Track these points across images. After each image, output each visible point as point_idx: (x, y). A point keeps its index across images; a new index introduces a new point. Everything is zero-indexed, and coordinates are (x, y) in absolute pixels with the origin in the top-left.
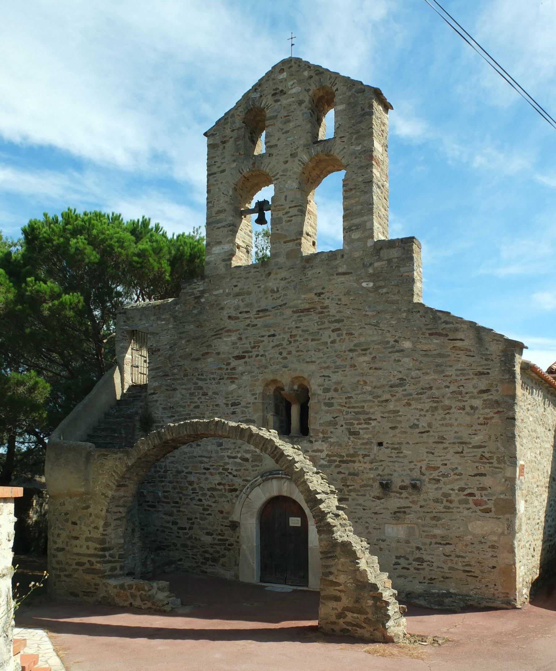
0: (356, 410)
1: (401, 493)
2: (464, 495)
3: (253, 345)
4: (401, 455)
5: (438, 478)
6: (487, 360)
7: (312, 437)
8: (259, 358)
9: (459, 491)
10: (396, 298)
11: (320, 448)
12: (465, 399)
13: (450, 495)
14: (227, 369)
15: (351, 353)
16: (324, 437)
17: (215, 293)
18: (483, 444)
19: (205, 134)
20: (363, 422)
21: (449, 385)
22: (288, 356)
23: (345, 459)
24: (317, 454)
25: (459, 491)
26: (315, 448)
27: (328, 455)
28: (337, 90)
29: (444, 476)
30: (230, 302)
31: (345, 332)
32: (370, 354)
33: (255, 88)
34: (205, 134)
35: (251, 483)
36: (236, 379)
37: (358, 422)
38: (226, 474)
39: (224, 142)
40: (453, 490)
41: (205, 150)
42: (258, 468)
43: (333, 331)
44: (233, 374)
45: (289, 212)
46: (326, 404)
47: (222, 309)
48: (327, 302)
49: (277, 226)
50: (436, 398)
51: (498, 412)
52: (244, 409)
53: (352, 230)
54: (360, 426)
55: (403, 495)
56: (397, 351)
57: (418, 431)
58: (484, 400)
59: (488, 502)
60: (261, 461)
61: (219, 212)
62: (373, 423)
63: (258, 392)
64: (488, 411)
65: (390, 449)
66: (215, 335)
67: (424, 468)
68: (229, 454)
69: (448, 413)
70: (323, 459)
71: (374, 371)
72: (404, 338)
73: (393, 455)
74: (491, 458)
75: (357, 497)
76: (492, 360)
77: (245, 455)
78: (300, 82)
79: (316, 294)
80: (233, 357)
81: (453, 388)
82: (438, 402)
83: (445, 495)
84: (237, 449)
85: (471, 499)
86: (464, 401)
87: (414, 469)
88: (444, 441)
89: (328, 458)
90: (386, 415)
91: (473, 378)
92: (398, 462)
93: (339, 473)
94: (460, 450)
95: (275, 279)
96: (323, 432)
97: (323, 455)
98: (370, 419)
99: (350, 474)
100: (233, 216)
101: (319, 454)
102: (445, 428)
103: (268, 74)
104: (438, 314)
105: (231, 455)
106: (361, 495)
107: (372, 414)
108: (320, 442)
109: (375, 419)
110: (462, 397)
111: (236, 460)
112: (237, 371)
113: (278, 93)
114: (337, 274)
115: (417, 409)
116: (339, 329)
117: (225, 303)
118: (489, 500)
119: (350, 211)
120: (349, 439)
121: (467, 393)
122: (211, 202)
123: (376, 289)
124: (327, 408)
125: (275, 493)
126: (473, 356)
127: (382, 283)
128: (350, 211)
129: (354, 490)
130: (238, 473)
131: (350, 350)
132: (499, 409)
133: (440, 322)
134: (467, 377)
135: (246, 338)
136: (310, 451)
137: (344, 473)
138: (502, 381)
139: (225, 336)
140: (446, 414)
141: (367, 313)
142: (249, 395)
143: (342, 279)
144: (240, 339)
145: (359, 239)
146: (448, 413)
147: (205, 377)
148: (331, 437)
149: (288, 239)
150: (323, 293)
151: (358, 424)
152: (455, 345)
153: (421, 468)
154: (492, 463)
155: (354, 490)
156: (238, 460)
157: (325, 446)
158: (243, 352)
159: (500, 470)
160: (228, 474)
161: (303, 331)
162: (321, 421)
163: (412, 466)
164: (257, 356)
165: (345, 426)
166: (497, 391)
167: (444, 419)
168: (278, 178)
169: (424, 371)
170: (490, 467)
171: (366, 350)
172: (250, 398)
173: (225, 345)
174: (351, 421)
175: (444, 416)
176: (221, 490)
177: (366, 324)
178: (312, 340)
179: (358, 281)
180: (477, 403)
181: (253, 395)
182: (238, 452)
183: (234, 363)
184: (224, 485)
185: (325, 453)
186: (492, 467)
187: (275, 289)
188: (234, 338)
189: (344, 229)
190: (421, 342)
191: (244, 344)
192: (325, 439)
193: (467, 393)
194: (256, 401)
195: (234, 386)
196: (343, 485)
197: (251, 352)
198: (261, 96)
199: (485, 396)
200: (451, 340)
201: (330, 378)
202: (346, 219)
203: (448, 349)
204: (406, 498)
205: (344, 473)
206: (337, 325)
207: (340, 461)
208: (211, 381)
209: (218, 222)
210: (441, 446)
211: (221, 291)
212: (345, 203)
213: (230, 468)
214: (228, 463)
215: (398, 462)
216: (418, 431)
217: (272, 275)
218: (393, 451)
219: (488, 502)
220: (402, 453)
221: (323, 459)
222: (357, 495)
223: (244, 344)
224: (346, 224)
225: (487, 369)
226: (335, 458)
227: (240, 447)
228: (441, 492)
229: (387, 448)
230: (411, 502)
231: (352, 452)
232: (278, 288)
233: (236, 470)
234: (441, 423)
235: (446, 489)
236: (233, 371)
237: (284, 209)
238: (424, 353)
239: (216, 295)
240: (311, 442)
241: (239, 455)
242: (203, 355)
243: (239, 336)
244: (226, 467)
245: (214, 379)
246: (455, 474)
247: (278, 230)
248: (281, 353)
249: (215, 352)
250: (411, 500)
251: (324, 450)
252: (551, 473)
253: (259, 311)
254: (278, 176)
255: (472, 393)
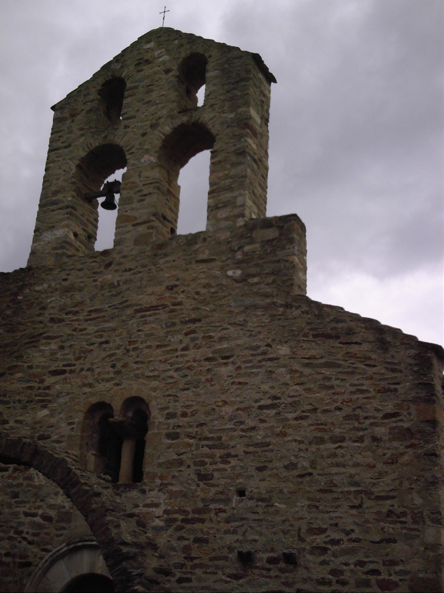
0: (210, 443)
1: (269, 570)
2: (364, 573)
3: (77, 355)
4: (271, 510)
5: (324, 545)
6: (393, 371)
7: (145, 484)
8: (84, 373)
9: (355, 565)
10: (268, 290)
11: (155, 501)
12: (363, 426)
13: (342, 572)
14: (39, 388)
15: (207, 363)
16: (162, 484)
17: (38, 288)
18: (391, 494)
19: (53, 108)
20: (219, 460)
21: (341, 406)
22: (123, 370)
23: (190, 516)
24: (151, 509)
25: (355, 565)
26: (148, 501)
27: (166, 512)
28: (210, 56)
29: (334, 542)
30: (54, 301)
31: (202, 335)
32: (233, 363)
33: (117, 59)
34: (53, 108)
35: (51, 553)
36: (50, 401)
37: (211, 460)
38: (19, 539)
39: (73, 116)
40: (346, 564)
41: (50, 123)
42: (64, 532)
43: (186, 334)
44: (47, 395)
45: (142, 190)
46: (169, 436)
47: (44, 308)
48: (181, 297)
49: (126, 206)
50: (322, 424)
51: (412, 446)
52: (55, 445)
53: (219, 208)
54: (215, 467)
55: (272, 573)
56: (271, 359)
57: (296, 472)
58: (392, 429)
59: (400, 583)
60: (69, 521)
61: (55, 193)
62: (233, 462)
63: (76, 420)
64: (395, 444)
65: (255, 500)
66: (29, 343)
67: (303, 530)
68: (26, 509)
69: (340, 447)
70: (158, 517)
71: (238, 386)
72: (280, 341)
73: (260, 510)
74: (404, 514)
75: (203, 575)
76: (401, 371)
77: (48, 511)
78: (168, 51)
79: (167, 287)
80: (50, 372)
81: (347, 410)
82: (325, 430)
83: (334, 572)
84: (39, 503)
85: (373, 578)
86: (362, 429)
87: (289, 531)
88: (334, 489)
89: (165, 516)
90: (251, 449)
91: (374, 397)
92: (266, 520)
93: (181, 538)
94: (356, 502)
95: (116, 271)
96: (161, 478)
97: (158, 511)
98: (228, 455)
99: (196, 540)
100: (73, 197)
101: (154, 509)
102: (335, 470)
103: (134, 45)
104: (325, 309)
105: (29, 511)
106: (210, 573)
107: (233, 447)
108: (156, 492)
109: (236, 456)
110: (359, 423)
111: (35, 519)
112: (53, 391)
113: (142, 62)
114: (197, 262)
115: (296, 441)
116: (194, 332)
117: (49, 301)
118: (401, 580)
119: (218, 186)
120: (198, 485)
121: (366, 418)
122: (48, 181)
123: (243, 280)
124: (169, 441)
125: (85, 570)
126: (374, 366)
127: (254, 270)
128: (218, 186)
129: (200, 566)
130: (36, 539)
131: (208, 359)
132: (413, 441)
133: (328, 320)
134: (366, 395)
135: (71, 346)
136: (141, 505)
137: (188, 539)
138: (415, 401)
139: (43, 344)
140: (337, 448)
141: (232, 309)
142: (63, 425)
143: (202, 266)
144: (62, 348)
145: (226, 219)
146: (340, 447)
147: (7, 399)
148: (171, 484)
149: (139, 221)
150: (176, 286)
151: (211, 464)
152: (349, 350)
153: (299, 530)
154: (405, 522)
155: (200, 566)
156: (38, 519)
157: (162, 498)
158: (64, 366)
159: (417, 533)
160: (22, 540)
161: (146, 335)
162: (161, 461)
163: (286, 527)
164: (82, 370)
165: (193, 467)
166: (410, 414)
167: (335, 455)
168: (133, 153)
169: (307, 386)
170: (401, 528)
171: (227, 357)
172: (65, 429)
173: (38, 358)
174: (203, 459)
175: (334, 451)
176: (8, 564)
177: (229, 324)
178: (158, 347)
179: (223, 269)
180: (380, 431)
181: (70, 424)
182: (39, 507)
183: (49, 380)
184: (14, 556)
185: (163, 507)
186: (405, 528)
187: (116, 284)
188: (54, 346)
189: (209, 207)
190: (302, 347)
191: (66, 354)
192: (162, 487)
193: (366, 418)
194: (73, 433)
195: (45, 412)
196: (185, 558)
197: (74, 365)
198: (122, 67)
199: (392, 423)
200: (344, 344)
201: (176, 398)
202: (210, 196)
203: (340, 356)
204: (276, 577)
205: (188, 539)
206: (192, 326)
207: (183, 521)
208: (16, 405)
209: (54, 203)
210: (329, 496)
211: (46, 285)
212: (212, 177)
213: (25, 530)
214: (23, 524)
215: (266, 520)
216: (296, 472)
217: (113, 266)
218: (260, 503)
219: (400, 583)
220: (272, 506)
221: (158, 517)
222: (206, 573)
223: (66, 354)
224: (211, 200)
225: (394, 384)
226: (176, 516)
227: (42, 501)
228: (328, 568)
229: (251, 498)
230: (283, 583)
231: (201, 505)
232: (118, 281)
233: (34, 535)
234: (329, 461)
235: (336, 563)
236: (47, 391)
237: (136, 187)
238: (306, 361)
239: (38, 292)
240: (143, 492)
241: (40, 512)
242: (10, 368)
243: (61, 344)
244: (21, 529)
245: (19, 401)
246: (351, 540)
247: (126, 211)
248: (113, 366)
249: (26, 365)
250: (283, 580)
251: (160, 504)
252: (65, 551)
253: (91, 311)
254: (134, 150)
255: (374, 418)
